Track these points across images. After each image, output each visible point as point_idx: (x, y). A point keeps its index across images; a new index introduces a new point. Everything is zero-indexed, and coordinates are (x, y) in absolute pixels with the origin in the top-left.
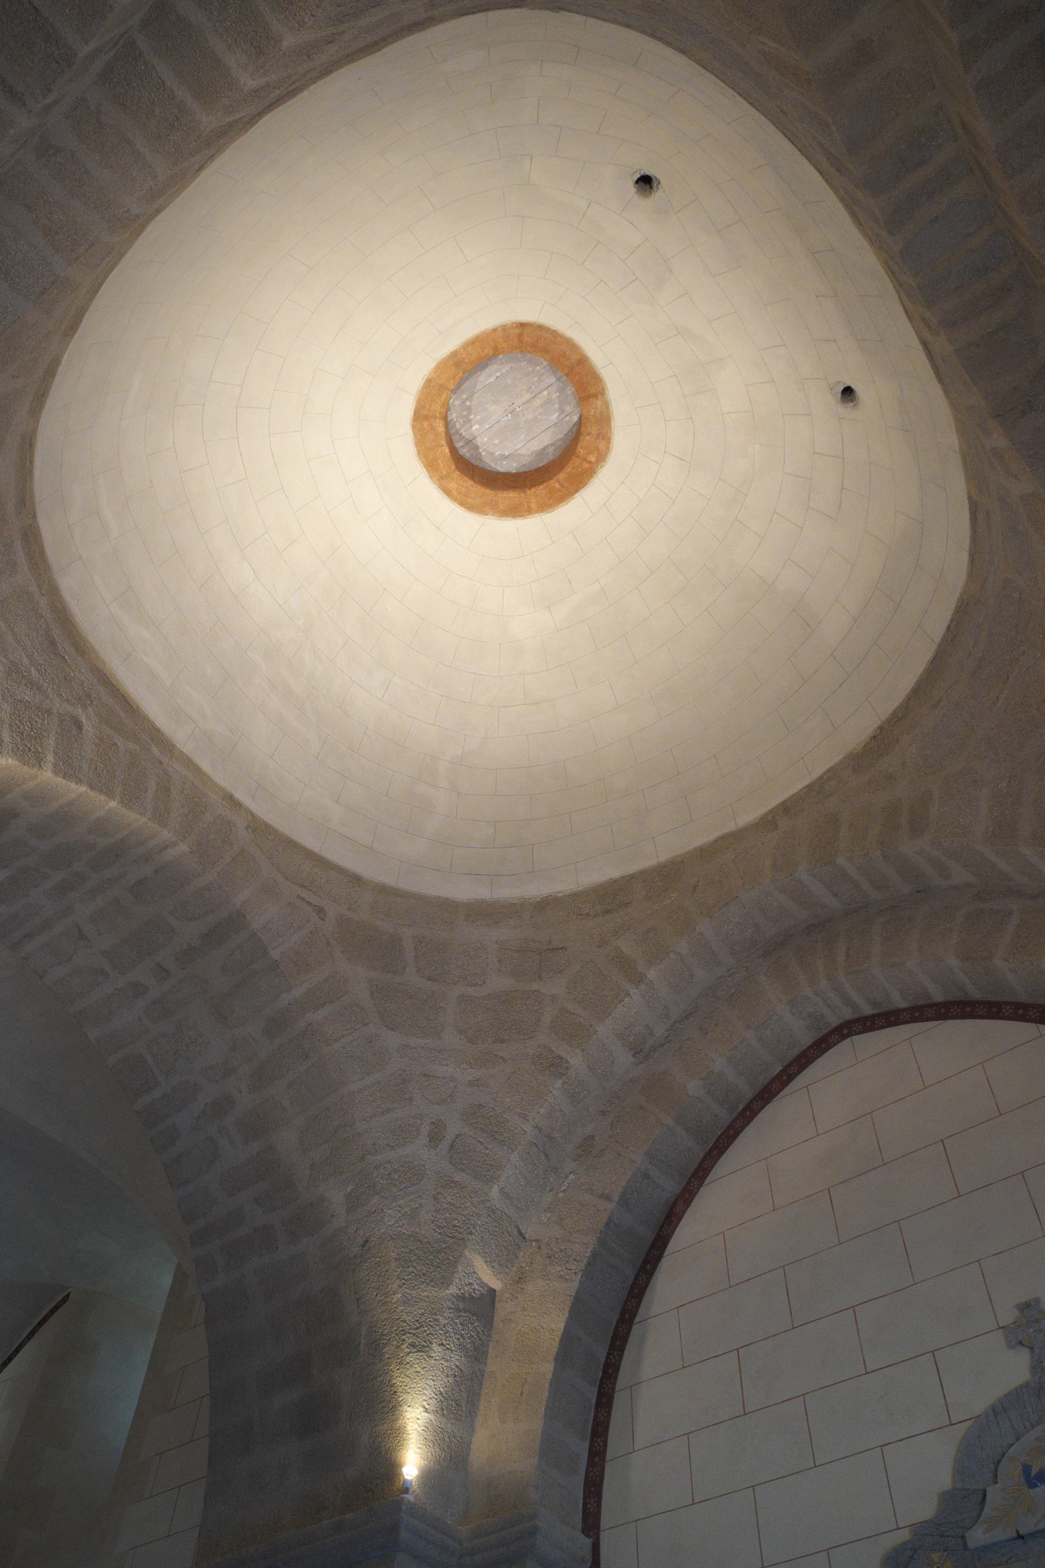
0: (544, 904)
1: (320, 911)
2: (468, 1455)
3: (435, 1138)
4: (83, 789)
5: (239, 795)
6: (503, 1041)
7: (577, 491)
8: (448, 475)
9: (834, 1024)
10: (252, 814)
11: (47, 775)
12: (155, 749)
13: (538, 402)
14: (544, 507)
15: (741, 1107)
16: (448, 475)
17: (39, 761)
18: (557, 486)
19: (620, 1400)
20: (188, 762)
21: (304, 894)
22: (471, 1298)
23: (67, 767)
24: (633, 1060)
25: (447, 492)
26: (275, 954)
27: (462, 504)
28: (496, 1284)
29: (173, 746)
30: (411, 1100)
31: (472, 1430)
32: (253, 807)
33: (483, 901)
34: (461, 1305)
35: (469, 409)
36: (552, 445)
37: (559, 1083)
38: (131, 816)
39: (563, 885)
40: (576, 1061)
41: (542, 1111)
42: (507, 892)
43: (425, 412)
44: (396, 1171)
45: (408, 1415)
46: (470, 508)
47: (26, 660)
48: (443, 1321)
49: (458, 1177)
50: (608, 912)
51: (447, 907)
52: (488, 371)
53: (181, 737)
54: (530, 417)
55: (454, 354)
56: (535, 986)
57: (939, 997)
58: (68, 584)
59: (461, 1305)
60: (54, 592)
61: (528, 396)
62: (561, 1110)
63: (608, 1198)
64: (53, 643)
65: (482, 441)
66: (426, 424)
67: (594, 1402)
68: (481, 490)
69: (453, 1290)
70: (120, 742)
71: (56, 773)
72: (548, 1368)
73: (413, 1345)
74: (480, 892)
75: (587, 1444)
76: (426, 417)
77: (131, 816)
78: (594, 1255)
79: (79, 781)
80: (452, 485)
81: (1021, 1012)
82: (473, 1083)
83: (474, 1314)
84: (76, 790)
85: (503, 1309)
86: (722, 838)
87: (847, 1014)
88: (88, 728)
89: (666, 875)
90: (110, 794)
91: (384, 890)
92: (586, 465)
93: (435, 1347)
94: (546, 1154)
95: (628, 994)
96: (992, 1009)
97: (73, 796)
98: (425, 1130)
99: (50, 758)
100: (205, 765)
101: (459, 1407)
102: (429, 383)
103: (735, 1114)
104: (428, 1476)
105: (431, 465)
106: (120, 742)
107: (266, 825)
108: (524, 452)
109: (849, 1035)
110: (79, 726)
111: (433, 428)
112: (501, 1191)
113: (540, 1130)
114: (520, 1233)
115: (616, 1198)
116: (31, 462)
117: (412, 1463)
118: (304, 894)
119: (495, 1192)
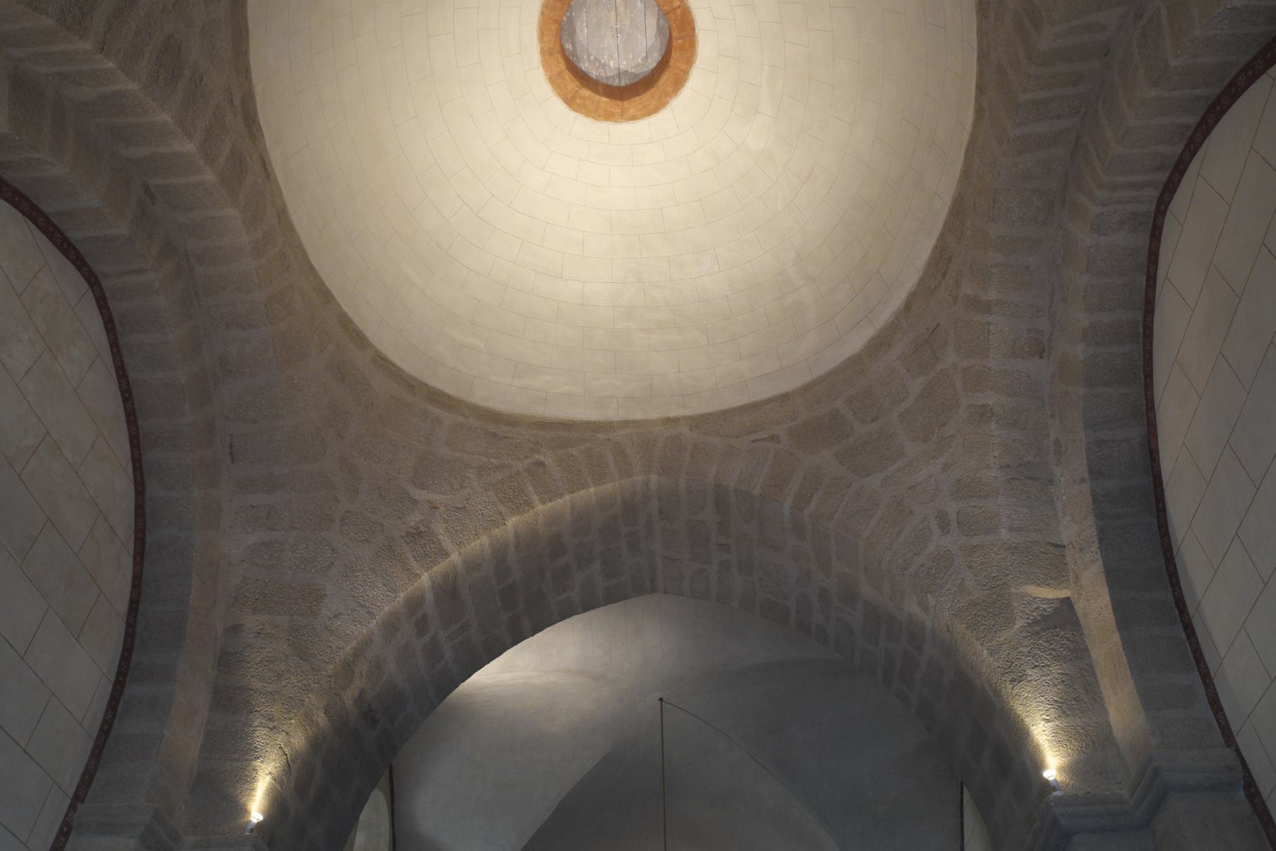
0: (908, 306)
1: (774, 438)
2: (1111, 732)
3: (944, 527)
4: (567, 497)
5: (672, 414)
6: (944, 424)
7: (693, 30)
8: (623, 110)
9: (1153, 208)
10: (689, 417)
11: (540, 508)
12: (600, 436)
13: (621, 9)
14: (690, 61)
15: (1141, 330)
16: (623, 110)
17: (530, 504)
18: (680, 41)
19: (1196, 622)
20: (626, 423)
21: (754, 437)
22: (1045, 618)
23: (549, 493)
24: (1044, 361)
25: (634, 118)
26: (757, 492)
27: (649, 114)
28: (1063, 594)
29: (612, 422)
30: (911, 512)
31: (1105, 712)
32: (687, 412)
33: (872, 338)
34: (1037, 629)
35: (596, 59)
36: (658, 20)
37: (993, 425)
38: (609, 487)
39: (910, 281)
40: (990, 399)
41: (996, 453)
42: (883, 317)
43: (569, 96)
44: (930, 568)
45: (1035, 732)
46: (656, 110)
47: (484, 459)
48: (1026, 650)
49: (975, 542)
50: (944, 274)
51: (854, 364)
52: (578, 31)
53: (612, 413)
54: (628, 22)
55: (543, 52)
56: (939, 368)
57: (1193, 120)
58: (479, 396)
59: (1037, 629)
60: (475, 409)
61: (613, 13)
62: (1014, 441)
63: (1083, 481)
64: (495, 435)
65: (624, 65)
66: (578, 101)
67: (1184, 636)
68: (647, 95)
69: (1020, 623)
70: (574, 451)
71: (544, 503)
72: (1116, 637)
73: (1013, 680)
74: (868, 333)
75: (1196, 672)
76: (574, 97)
77: (609, 487)
78: (1101, 530)
79: (561, 496)
80: (632, 111)
81: (1250, 73)
82: (946, 468)
83: (1055, 627)
84: (563, 502)
85: (1079, 606)
86: (967, 151)
87: (1156, 193)
88: (549, 461)
89: (958, 210)
90: (584, 486)
91: (806, 388)
92: (679, 11)
93: (1029, 672)
94: (1031, 478)
95: (989, 324)
96: (1233, 92)
97: (569, 504)
98: (934, 525)
99: (535, 498)
100: (639, 416)
101: (1079, 701)
102: (551, 80)
103: (1141, 340)
104: (1074, 769)
105: (608, 117)
106: (574, 451)
107: (703, 416)
108: (650, 43)
109: (1166, 207)
110: (541, 464)
111: (584, 98)
112: (1011, 529)
113: (1008, 466)
114: (1056, 546)
115: (1087, 477)
116: (394, 365)
117: (1053, 766)
118: (754, 437)
119: (1003, 532)
